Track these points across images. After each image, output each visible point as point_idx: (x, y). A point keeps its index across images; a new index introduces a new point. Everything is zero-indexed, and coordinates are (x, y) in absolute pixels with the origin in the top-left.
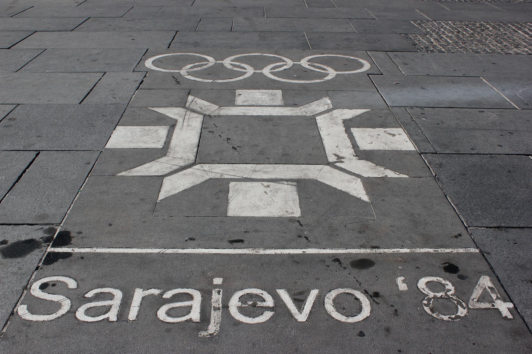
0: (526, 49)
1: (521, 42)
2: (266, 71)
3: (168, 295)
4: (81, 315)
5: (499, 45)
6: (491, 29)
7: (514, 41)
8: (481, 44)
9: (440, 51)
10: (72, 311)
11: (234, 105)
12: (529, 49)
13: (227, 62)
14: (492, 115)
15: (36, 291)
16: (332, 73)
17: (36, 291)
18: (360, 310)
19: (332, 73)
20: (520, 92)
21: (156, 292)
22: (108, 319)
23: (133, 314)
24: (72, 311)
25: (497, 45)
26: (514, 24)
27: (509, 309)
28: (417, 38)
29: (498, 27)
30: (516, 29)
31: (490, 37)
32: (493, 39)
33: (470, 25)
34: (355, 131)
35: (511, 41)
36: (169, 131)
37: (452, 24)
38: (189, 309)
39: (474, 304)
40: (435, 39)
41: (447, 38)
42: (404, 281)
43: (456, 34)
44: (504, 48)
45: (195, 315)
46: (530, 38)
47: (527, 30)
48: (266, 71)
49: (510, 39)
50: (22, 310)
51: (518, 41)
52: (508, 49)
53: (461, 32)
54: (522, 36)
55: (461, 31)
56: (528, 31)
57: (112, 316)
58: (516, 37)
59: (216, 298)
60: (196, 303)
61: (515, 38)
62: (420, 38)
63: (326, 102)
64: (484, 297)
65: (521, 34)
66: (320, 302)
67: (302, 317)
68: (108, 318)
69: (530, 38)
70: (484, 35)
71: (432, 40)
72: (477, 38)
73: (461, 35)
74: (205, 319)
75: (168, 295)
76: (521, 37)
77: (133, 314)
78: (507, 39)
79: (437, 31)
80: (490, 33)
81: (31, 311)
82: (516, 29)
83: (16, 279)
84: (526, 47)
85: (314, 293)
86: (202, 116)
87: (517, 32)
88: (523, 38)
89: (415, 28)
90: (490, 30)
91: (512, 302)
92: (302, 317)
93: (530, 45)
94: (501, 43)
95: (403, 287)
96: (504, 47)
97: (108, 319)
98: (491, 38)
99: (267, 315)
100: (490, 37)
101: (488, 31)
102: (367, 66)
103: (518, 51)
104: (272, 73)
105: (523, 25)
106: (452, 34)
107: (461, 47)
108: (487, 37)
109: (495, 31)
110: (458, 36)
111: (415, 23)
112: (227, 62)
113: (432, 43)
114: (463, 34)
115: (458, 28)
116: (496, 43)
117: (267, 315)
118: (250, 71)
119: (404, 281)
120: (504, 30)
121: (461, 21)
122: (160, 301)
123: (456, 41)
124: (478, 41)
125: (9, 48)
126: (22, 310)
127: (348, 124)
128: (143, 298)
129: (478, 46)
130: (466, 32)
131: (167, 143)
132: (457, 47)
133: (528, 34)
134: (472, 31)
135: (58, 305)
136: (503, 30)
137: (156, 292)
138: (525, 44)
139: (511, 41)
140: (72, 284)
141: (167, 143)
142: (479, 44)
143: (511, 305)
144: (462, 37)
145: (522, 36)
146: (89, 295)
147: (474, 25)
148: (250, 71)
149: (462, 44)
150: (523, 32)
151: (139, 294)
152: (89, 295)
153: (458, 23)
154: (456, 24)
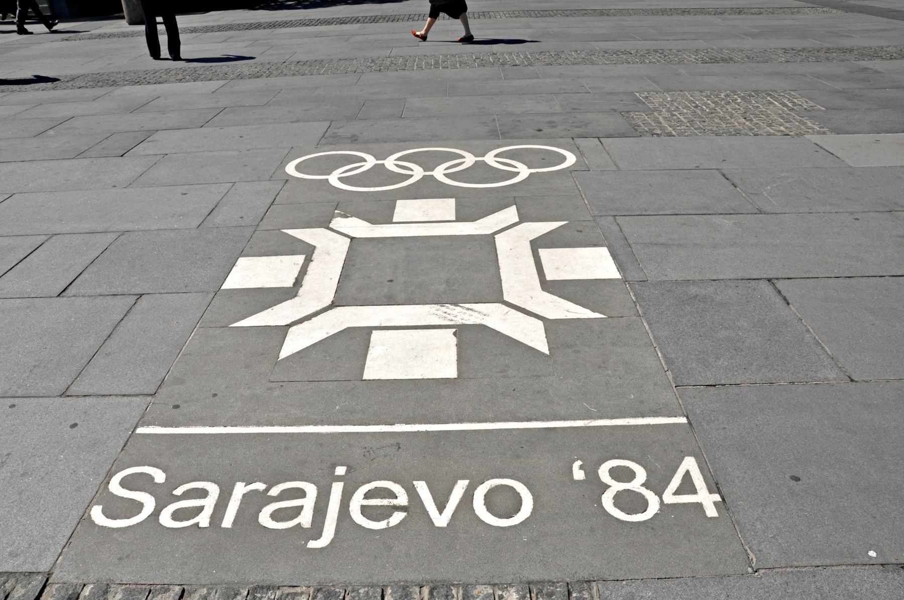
0: (782, 128)
1: (776, 118)
2: (439, 173)
3: (275, 491)
4: (165, 519)
5: (747, 123)
6: (739, 100)
7: (768, 117)
8: (724, 123)
9: (670, 135)
10: (156, 514)
11: (390, 222)
12: (786, 128)
13: (390, 163)
14: (727, 223)
15: (115, 487)
16: (524, 172)
17: (115, 487)
18: (517, 507)
19: (524, 172)
20: (768, 189)
21: (260, 486)
22: (197, 524)
23: (227, 522)
24: (156, 514)
25: (744, 124)
26: (771, 93)
27: (716, 504)
28: (642, 117)
29: (748, 98)
30: (771, 100)
31: (737, 112)
32: (741, 115)
33: (712, 96)
34: (543, 253)
35: (763, 116)
36: (305, 260)
37: (689, 96)
38: (298, 510)
39: (669, 498)
40: (665, 118)
41: (680, 116)
42: (581, 468)
43: (693, 110)
44: (753, 127)
45: (305, 519)
46: (789, 112)
47: (785, 101)
48: (439, 173)
49: (762, 114)
50: (97, 514)
51: (773, 117)
52: (759, 128)
53: (700, 106)
54: (778, 109)
55: (700, 105)
56: (788, 103)
57: (203, 520)
58: (771, 111)
59: (337, 489)
60: (308, 503)
61: (769, 112)
62: (646, 117)
63: (510, 214)
64: (687, 486)
65: (778, 107)
66: (468, 497)
67: (441, 520)
68: (197, 524)
69: (789, 112)
70: (730, 110)
71: (661, 119)
72: (720, 115)
73: (700, 110)
74: (316, 530)
75: (275, 491)
76: (778, 110)
77: (227, 522)
78: (759, 115)
79: (668, 106)
80: (737, 106)
81: (108, 514)
82: (771, 100)
83: (93, 470)
84: (781, 125)
85: (461, 487)
86: (349, 240)
87: (774, 103)
88: (781, 112)
89: (639, 103)
90: (738, 103)
91: (720, 493)
92: (441, 520)
93: (787, 122)
94: (751, 120)
95: (579, 474)
96: (754, 126)
97: (197, 524)
98: (738, 114)
99: (397, 518)
100: (737, 112)
101: (736, 103)
102: (571, 159)
103: (772, 131)
104: (446, 175)
105: (782, 94)
106: (687, 110)
107: (698, 128)
108: (733, 112)
109: (744, 104)
110: (695, 112)
111: (640, 96)
112: (390, 163)
113: (660, 123)
114: (702, 110)
115: (696, 100)
116: (743, 120)
117: (397, 518)
118: (418, 173)
119: (581, 468)
120: (756, 102)
121: (701, 92)
122: (263, 499)
123: (691, 119)
124: (721, 118)
125: (122, 156)
126: (97, 514)
127: (536, 245)
128: (244, 495)
129: (721, 126)
130: (706, 107)
131: (298, 282)
132: (693, 128)
133: (787, 106)
134: (713, 105)
135: (139, 506)
136: (754, 102)
137: (260, 486)
138: (782, 120)
139: (763, 116)
140: (159, 476)
141: (298, 282)
142: (722, 123)
143: (717, 497)
144: (700, 113)
145: (778, 109)
146: (178, 492)
147: (717, 96)
148: (418, 173)
149: (699, 124)
150: (780, 104)
151: (240, 489)
152: (178, 492)
153: (697, 94)
154: (694, 95)
